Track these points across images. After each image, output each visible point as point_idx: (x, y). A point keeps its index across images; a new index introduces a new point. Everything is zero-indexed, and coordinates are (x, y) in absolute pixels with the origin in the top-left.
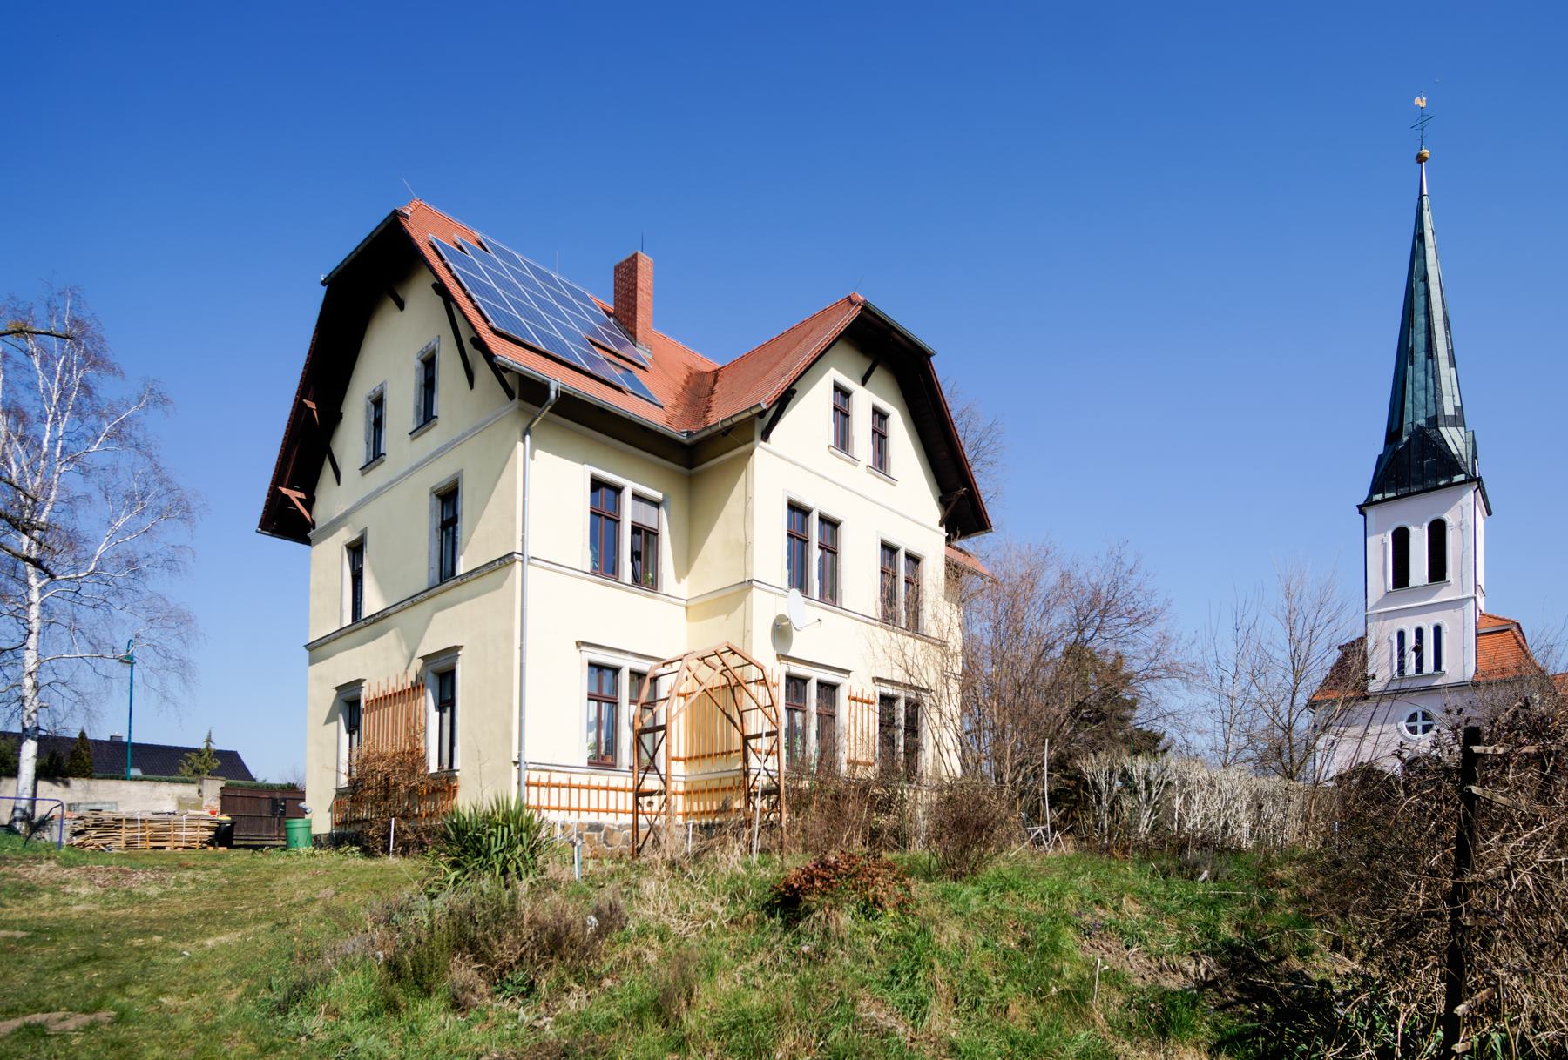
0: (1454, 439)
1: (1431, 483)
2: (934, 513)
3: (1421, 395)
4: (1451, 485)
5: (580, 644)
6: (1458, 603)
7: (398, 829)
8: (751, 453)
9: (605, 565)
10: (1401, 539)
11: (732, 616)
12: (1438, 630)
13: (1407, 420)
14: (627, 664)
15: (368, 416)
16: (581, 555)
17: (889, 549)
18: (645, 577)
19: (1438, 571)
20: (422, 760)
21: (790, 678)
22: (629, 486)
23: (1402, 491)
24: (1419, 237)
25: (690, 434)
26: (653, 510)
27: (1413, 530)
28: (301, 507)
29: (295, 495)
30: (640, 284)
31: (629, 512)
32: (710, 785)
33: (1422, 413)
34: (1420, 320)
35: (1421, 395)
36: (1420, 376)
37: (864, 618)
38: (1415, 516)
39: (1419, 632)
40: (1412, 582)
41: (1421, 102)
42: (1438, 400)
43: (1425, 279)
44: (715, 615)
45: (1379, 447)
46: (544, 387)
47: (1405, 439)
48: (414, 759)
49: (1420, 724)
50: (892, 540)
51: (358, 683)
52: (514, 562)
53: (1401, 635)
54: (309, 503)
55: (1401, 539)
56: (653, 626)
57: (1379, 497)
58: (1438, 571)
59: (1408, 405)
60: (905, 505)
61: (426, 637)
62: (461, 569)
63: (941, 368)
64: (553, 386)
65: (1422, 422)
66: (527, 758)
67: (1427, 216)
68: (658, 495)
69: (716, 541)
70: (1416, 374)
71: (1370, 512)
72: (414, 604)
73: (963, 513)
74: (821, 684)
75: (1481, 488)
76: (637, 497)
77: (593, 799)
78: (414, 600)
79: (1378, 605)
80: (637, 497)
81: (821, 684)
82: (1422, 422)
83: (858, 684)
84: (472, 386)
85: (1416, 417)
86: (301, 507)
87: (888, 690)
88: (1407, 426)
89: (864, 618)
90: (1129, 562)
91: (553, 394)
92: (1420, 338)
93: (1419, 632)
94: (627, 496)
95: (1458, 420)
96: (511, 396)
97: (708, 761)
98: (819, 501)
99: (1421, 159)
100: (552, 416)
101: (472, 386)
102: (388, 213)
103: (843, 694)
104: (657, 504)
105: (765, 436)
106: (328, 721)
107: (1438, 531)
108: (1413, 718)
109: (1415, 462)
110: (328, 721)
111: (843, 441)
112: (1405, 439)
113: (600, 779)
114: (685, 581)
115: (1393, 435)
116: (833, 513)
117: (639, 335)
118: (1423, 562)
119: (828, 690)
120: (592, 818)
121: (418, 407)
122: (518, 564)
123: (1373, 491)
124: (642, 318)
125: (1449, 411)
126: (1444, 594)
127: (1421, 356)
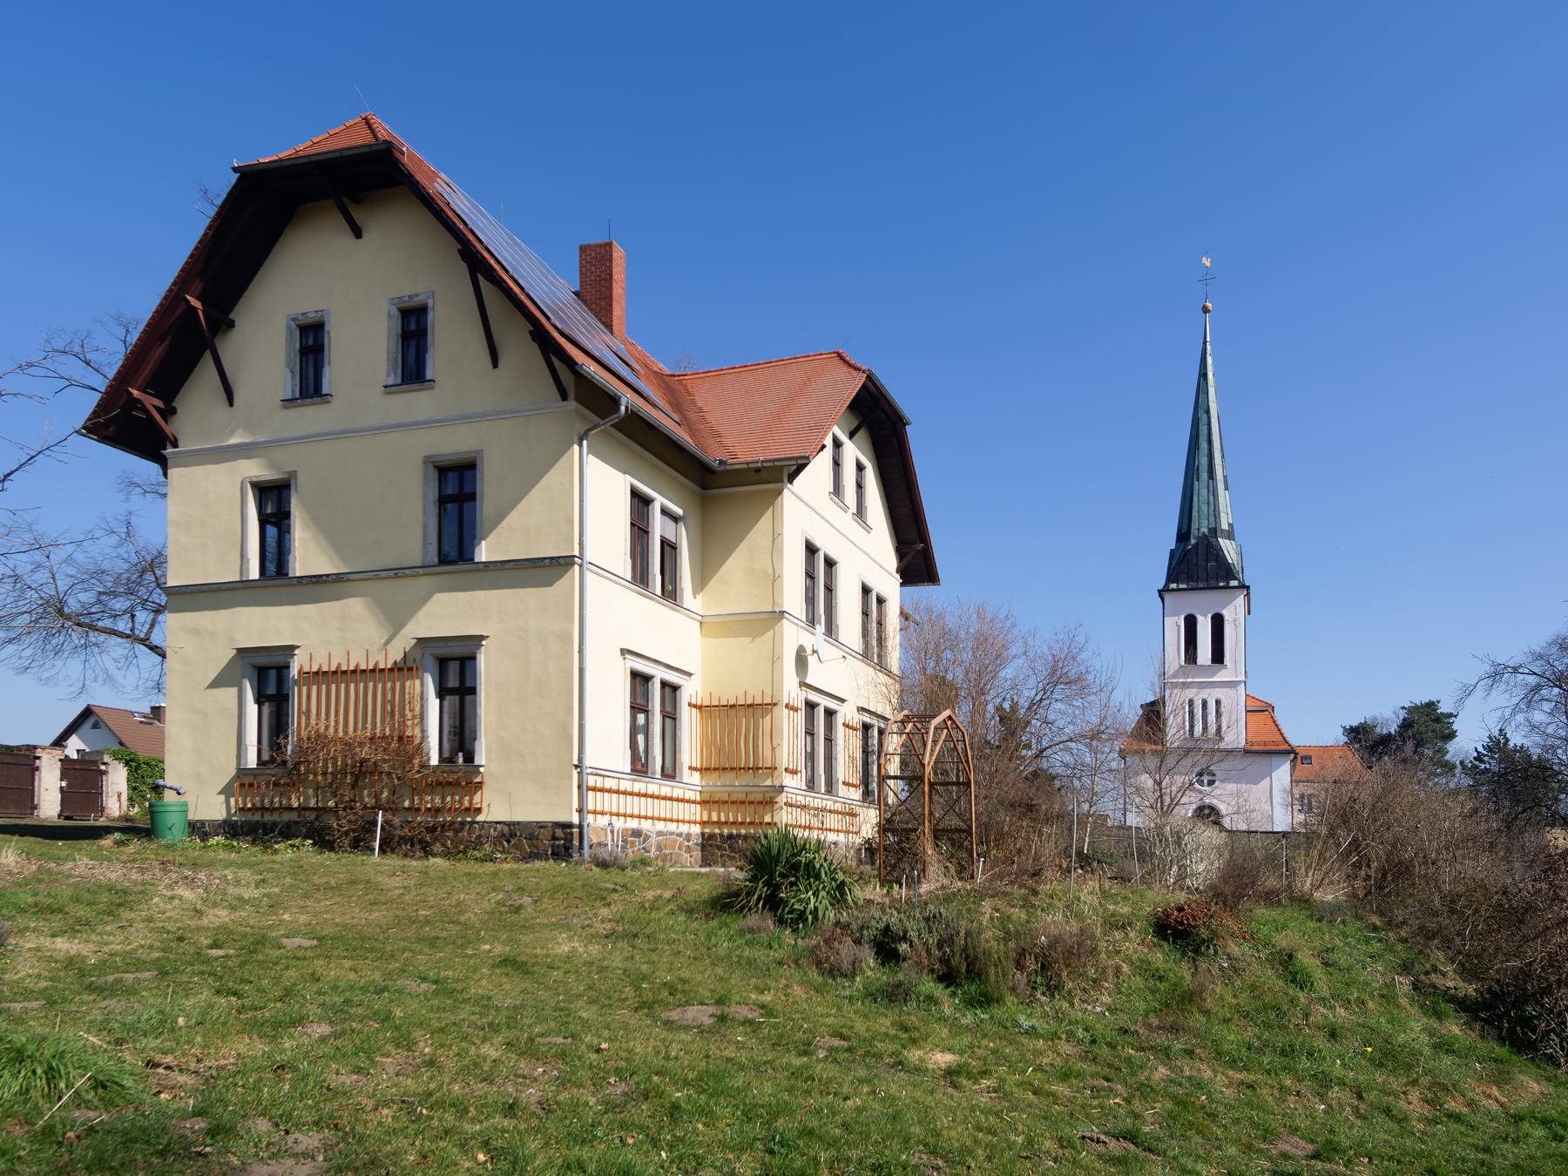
0: (1228, 548)
1: (1213, 583)
2: (892, 562)
3: (1204, 507)
4: (1227, 587)
5: (624, 652)
6: (1232, 684)
7: (386, 822)
8: (780, 492)
9: (640, 577)
10: (1191, 623)
11: (758, 640)
12: (1218, 702)
13: (1194, 526)
14: (660, 674)
15: (289, 341)
16: (624, 566)
17: (866, 591)
18: (670, 593)
19: (1218, 656)
20: (420, 749)
21: (635, 675)
22: (659, 500)
23: (1192, 584)
24: (1203, 375)
25: (721, 462)
26: (672, 524)
27: (1200, 618)
28: (158, 417)
29: (152, 402)
30: (615, 276)
31: (659, 527)
32: (734, 797)
33: (1205, 523)
34: (1204, 445)
35: (1204, 507)
36: (1204, 492)
37: (851, 652)
38: (1203, 606)
39: (1205, 703)
40: (1199, 661)
41: (1207, 262)
42: (1217, 516)
43: (1208, 412)
44: (736, 635)
45: (1172, 543)
46: (614, 401)
47: (1193, 541)
48: (406, 747)
49: (1206, 779)
50: (869, 584)
51: (290, 649)
52: (573, 564)
53: (1191, 703)
54: (169, 412)
55: (1191, 623)
56: (676, 637)
57: (1174, 586)
58: (1218, 656)
59: (1195, 514)
60: (868, 554)
61: (421, 615)
62: (485, 552)
63: (918, 440)
64: (623, 401)
65: (1205, 530)
66: (589, 761)
67: (1209, 360)
68: (680, 512)
69: (736, 565)
70: (1201, 488)
71: (1167, 597)
72: (377, 578)
73: (916, 564)
74: (664, 684)
75: (1248, 594)
76: (664, 512)
77: (633, 805)
78: (398, 572)
79: (1175, 675)
80: (664, 512)
81: (664, 684)
82: (1205, 530)
83: (847, 713)
84: (495, 365)
85: (1200, 526)
86: (158, 417)
87: (867, 719)
88: (1194, 531)
89: (851, 652)
90: (1081, 639)
91: (623, 408)
92: (1204, 461)
93: (1205, 703)
94: (656, 509)
95: (1230, 535)
96: (564, 397)
97: (731, 775)
98: (828, 545)
99: (1205, 310)
100: (614, 431)
101: (495, 365)
102: (1425, 700)
103: (839, 720)
104: (676, 519)
105: (791, 482)
106: (216, 683)
107: (1218, 622)
108: (1200, 774)
109: (1198, 564)
110: (216, 683)
111: (837, 490)
112: (1193, 541)
113: (639, 787)
114: (700, 597)
115: (1183, 536)
116: (834, 555)
117: (615, 329)
118: (1207, 645)
119: (670, 689)
120: (633, 824)
121: (395, 359)
122: (577, 568)
123: (1169, 579)
124: (617, 311)
125: (1225, 526)
126: (1222, 676)
127: (1204, 476)
